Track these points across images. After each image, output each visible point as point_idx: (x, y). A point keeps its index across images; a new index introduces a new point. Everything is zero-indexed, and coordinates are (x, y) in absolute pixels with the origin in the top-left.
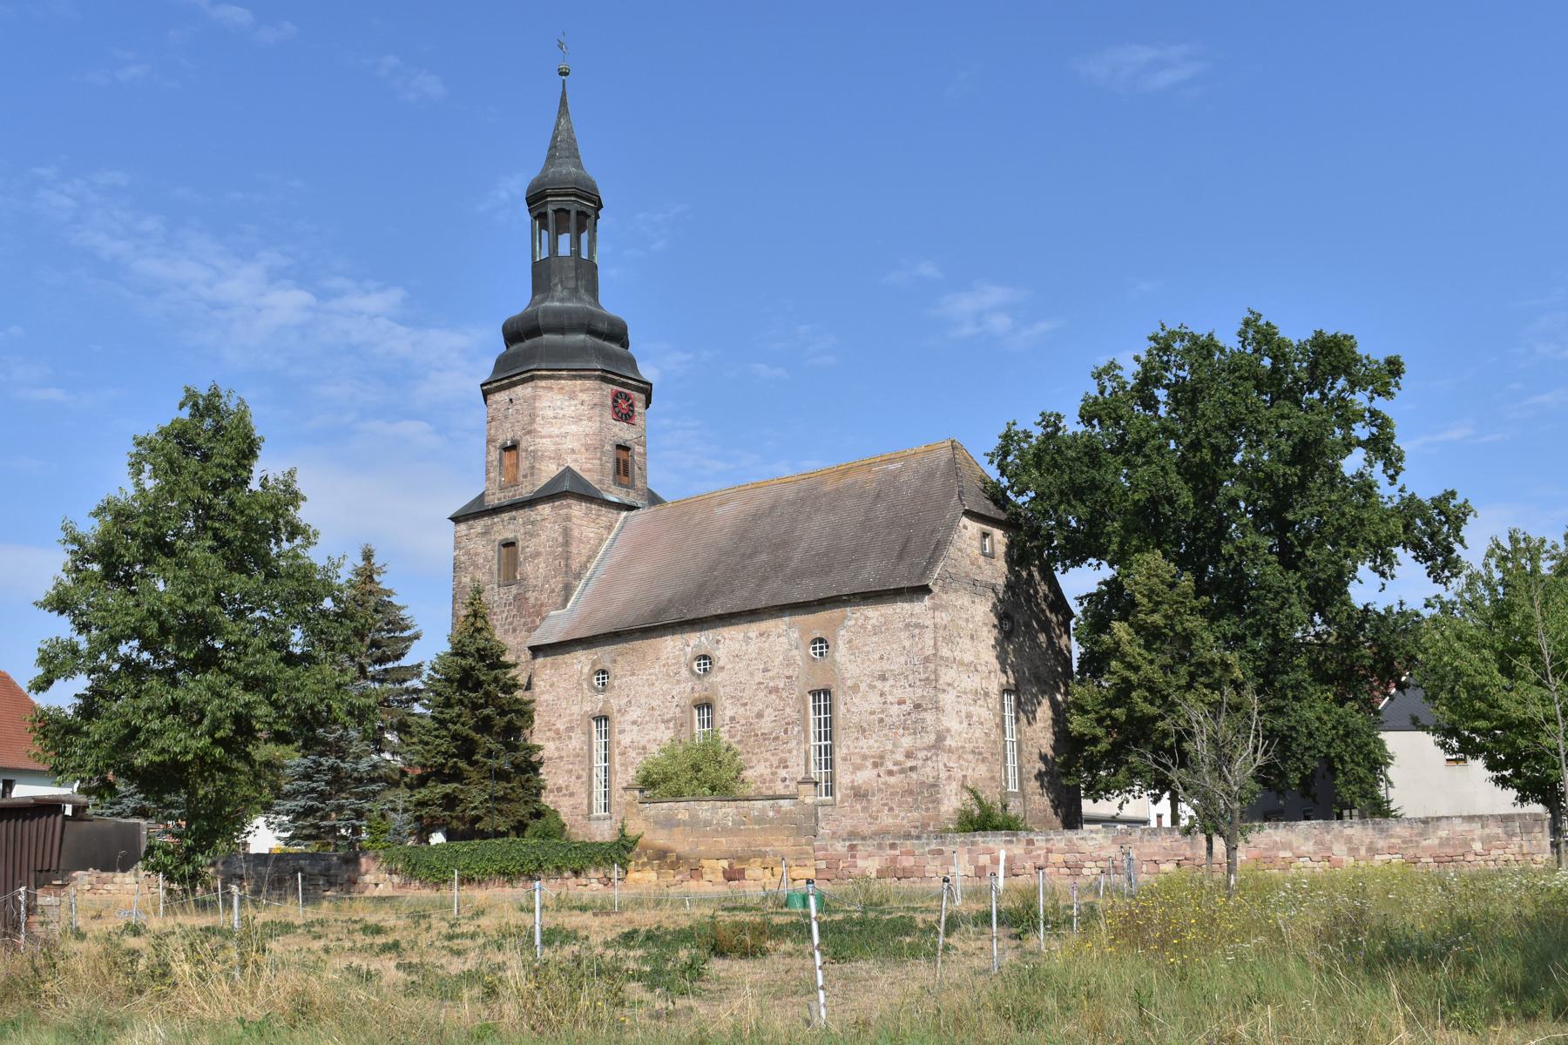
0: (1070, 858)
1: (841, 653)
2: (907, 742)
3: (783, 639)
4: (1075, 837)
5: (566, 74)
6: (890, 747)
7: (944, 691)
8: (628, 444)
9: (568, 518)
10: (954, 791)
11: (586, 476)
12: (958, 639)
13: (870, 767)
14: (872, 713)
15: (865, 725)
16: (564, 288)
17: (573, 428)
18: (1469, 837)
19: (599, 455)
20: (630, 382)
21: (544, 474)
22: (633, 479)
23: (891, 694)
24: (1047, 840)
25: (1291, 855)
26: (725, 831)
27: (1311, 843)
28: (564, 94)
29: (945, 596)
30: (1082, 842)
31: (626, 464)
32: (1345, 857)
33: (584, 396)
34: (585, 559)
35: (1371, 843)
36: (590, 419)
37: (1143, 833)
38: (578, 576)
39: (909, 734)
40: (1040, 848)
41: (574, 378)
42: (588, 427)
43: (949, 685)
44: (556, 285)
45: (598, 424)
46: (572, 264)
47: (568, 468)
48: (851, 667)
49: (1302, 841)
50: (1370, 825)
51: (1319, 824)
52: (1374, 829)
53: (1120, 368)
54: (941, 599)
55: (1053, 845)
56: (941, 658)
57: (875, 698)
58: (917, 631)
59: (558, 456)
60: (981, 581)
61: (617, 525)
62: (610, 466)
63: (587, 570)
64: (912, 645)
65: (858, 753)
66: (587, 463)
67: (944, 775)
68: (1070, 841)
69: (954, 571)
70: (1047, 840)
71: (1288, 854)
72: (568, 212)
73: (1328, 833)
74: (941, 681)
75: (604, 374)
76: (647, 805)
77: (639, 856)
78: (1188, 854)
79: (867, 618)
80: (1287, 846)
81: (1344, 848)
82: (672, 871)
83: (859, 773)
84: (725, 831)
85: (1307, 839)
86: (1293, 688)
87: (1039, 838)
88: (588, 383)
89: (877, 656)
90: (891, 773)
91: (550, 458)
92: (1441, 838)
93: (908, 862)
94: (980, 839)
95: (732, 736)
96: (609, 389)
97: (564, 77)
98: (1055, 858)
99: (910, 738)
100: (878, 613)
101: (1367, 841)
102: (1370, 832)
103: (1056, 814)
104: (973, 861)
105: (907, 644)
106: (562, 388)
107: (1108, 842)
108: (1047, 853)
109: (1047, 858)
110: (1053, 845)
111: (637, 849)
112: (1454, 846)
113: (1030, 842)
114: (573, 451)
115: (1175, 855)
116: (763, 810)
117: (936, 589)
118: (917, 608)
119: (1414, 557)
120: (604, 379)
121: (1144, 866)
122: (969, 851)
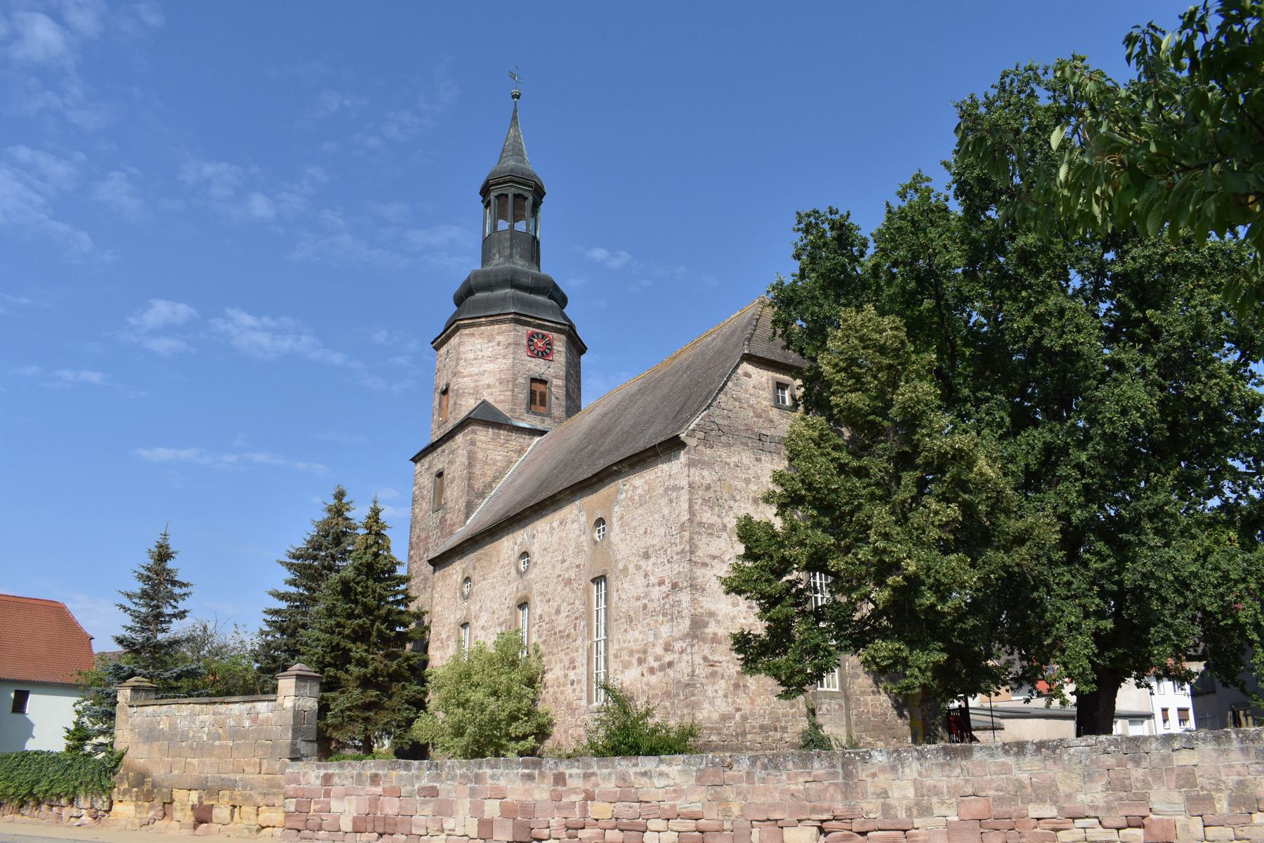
0: (626, 810)
1: (615, 532)
2: (665, 631)
3: (575, 525)
4: (632, 770)
5: (518, 97)
6: (651, 639)
7: (705, 565)
8: (544, 377)
9: (473, 443)
10: (721, 693)
11: (499, 407)
12: (732, 503)
13: (636, 664)
14: (638, 599)
15: (631, 613)
16: (501, 256)
17: (490, 366)
19: (511, 386)
20: (546, 323)
21: (464, 408)
22: (550, 410)
23: (653, 574)
24: (586, 776)
25: (1054, 812)
26: (201, 750)
27: (1099, 786)
28: (515, 111)
29: (708, 451)
30: (644, 780)
31: (543, 396)
32: (1181, 819)
33: (500, 338)
34: (489, 479)
35: (1241, 784)
36: (504, 357)
37: (753, 764)
38: (482, 495)
39: (668, 622)
40: (574, 791)
41: (492, 323)
42: (504, 363)
43: (714, 558)
44: (494, 255)
46: (508, 236)
47: (484, 402)
48: (622, 547)
49: (1077, 782)
50: (1236, 744)
52: (1245, 751)
53: (928, 180)
54: (702, 454)
55: (596, 785)
56: (701, 524)
57: (640, 581)
58: (674, 494)
59: (476, 391)
60: (773, 437)
61: (529, 449)
62: (523, 396)
63: (492, 490)
64: (670, 513)
65: (627, 648)
67: (702, 671)
68: (623, 778)
69: (726, 422)
70: (586, 776)
71: (1049, 811)
72: (506, 196)
73: (1137, 762)
74: (700, 553)
75: (517, 317)
76: (135, 709)
77: (121, 782)
78: (839, 807)
79: (635, 488)
80: (1045, 793)
81: (1178, 797)
82: (147, 804)
83: (627, 672)
84: (201, 750)
85: (1088, 777)
86: (1152, 516)
87: (575, 771)
88: (504, 327)
89: (642, 531)
90: (652, 671)
91: (470, 394)
93: (391, 807)
94: (488, 771)
95: (540, 637)
96: (525, 331)
98: (599, 809)
99: (668, 626)
100: (643, 480)
101: (1232, 780)
102: (1236, 758)
103: (901, 715)
104: (477, 810)
105: (666, 511)
107: (687, 782)
108: (586, 799)
109: (584, 810)
110: (596, 785)
111: (121, 771)
113: (560, 779)
114: (489, 386)
115: (814, 810)
116: (239, 719)
117: (692, 442)
118: (674, 467)
120: (517, 322)
121: (755, 831)
122: (473, 793)
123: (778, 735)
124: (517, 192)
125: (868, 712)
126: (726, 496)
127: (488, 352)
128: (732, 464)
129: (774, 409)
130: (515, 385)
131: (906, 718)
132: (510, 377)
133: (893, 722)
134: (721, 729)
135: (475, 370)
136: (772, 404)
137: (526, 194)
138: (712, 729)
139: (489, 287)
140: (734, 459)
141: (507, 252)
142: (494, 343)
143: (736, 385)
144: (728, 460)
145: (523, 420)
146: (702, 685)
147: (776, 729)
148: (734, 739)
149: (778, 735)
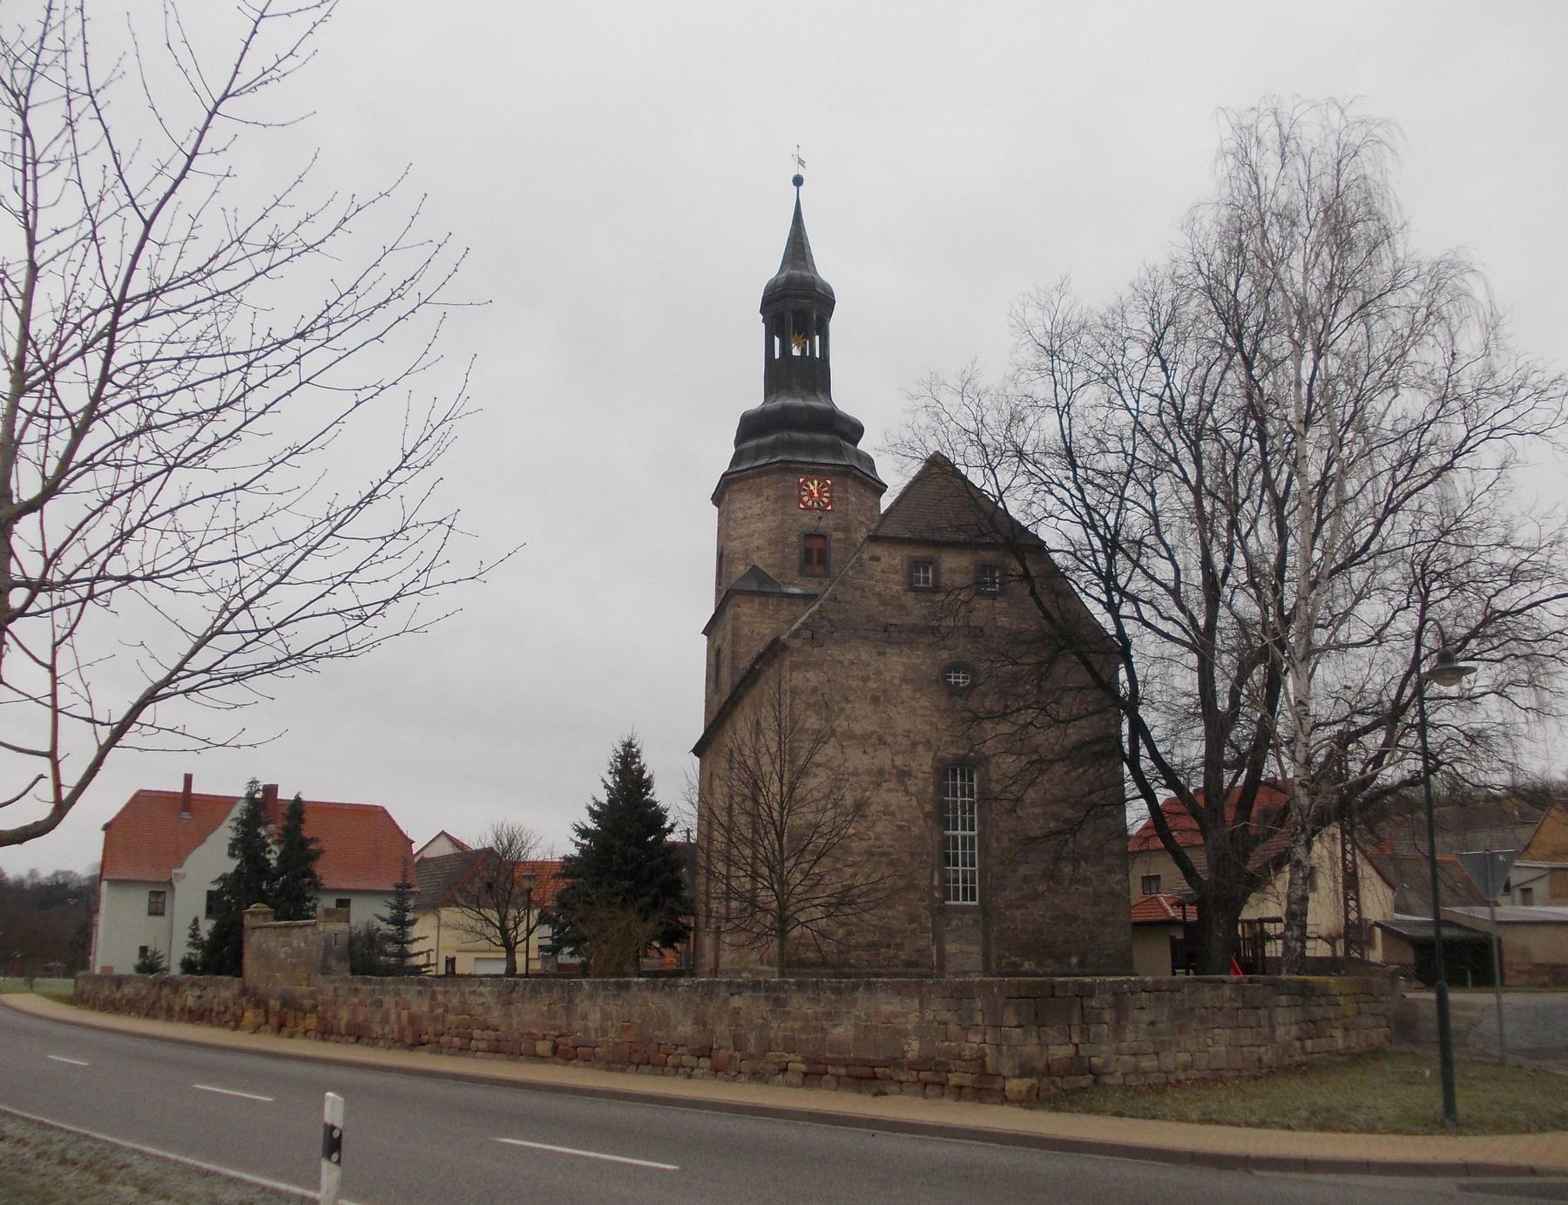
8: (821, 531)
29: (816, 651)
33: (769, 492)
62: (795, 557)
123: (892, 952)
125: (1016, 928)
126: (836, 698)
127: (756, 510)
129: (909, 594)
135: (743, 531)
136: (906, 587)
140: (850, 656)
142: (762, 498)
144: (841, 658)
147: (888, 946)
148: (835, 957)
149: (892, 952)
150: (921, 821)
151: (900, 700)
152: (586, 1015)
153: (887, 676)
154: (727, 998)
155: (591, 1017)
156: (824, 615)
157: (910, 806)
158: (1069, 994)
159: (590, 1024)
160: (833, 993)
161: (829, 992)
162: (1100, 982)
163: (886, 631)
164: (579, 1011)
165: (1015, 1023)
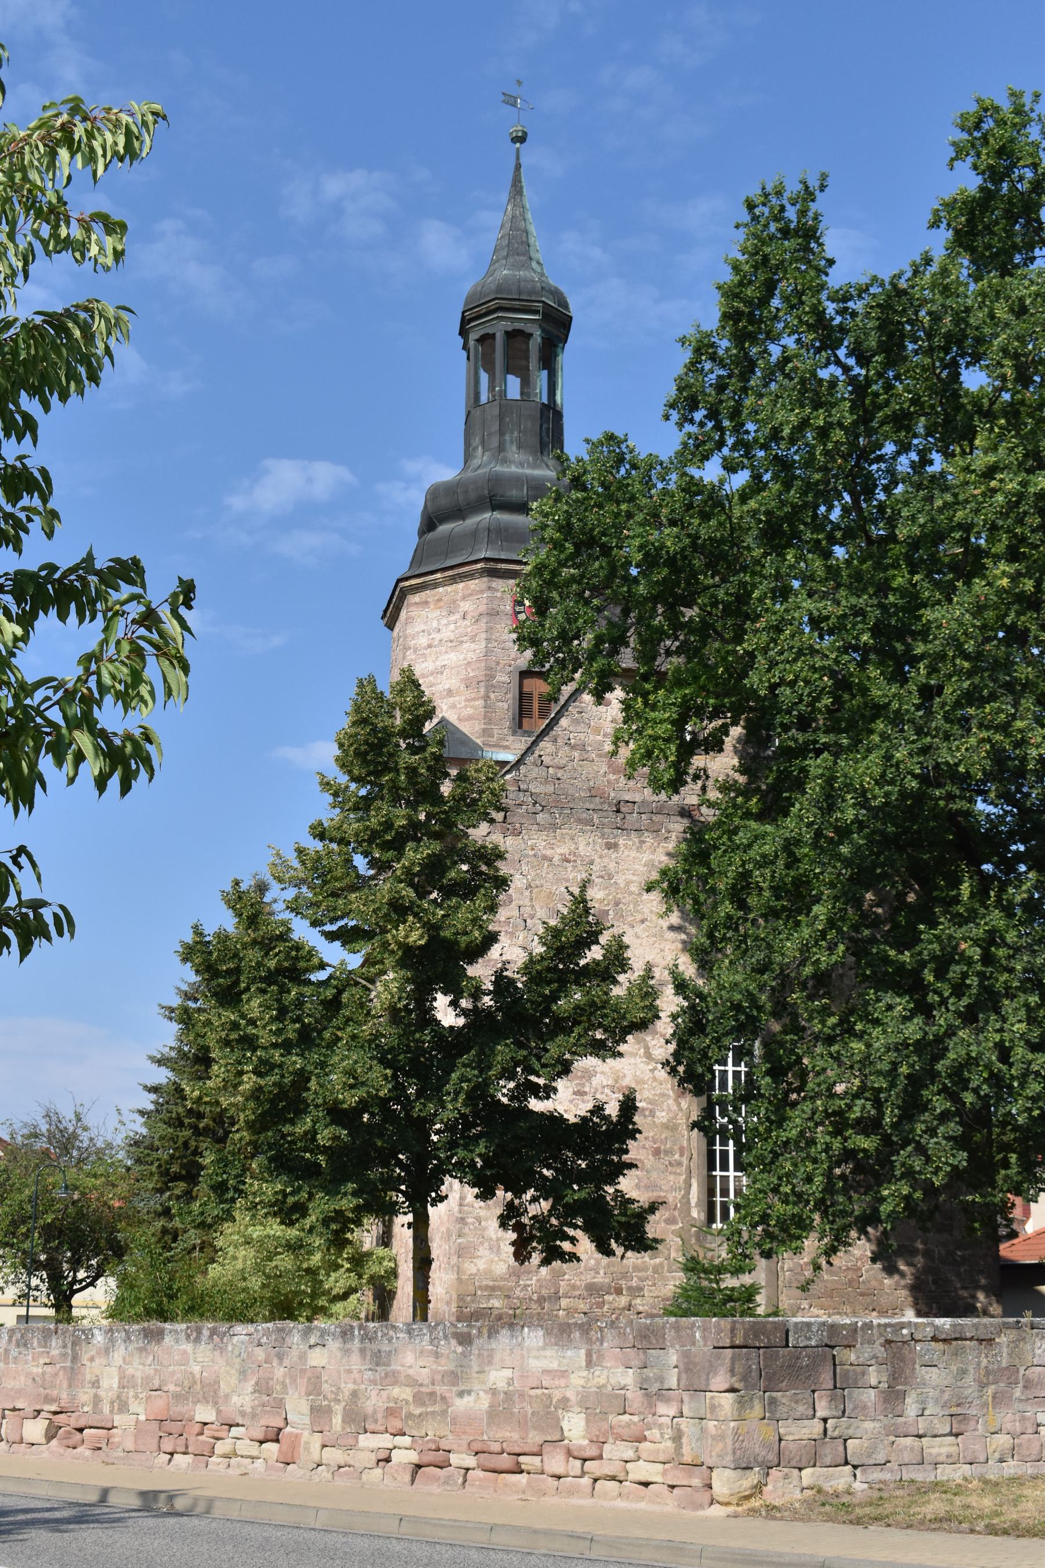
11: (466, 728)
17: (452, 658)
18: (557, 1395)
19: (482, 690)
28: (518, 167)
33: (465, 606)
36: (473, 639)
41: (454, 580)
42: (472, 651)
45: (484, 644)
51: (267, 1333)
62: (506, 705)
66: (466, 707)
69: (550, 789)
71: (205, 1413)
72: (493, 336)
88: (473, 584)
92: (494, 1392)
97: (518, 145)
106: (439, 600)
112: (522, 1424)
114: (450, 693)
119: (90, 558)
120: (493, 573)
123: (623, 1301)
124: (510, 326)
128: (556, 859)
130: (490, 687)
131: (903, 1275)
132: (481, 674)
133: (874, 1283)
134: (510, 1289)
137: (529, 328)
138: (493, 1289)
139: (458, 513)
140: (563, 849)
141: (495, 442)
142: (457, 616)
143: (576, 722)
144: (549, 853)
145: (506, 747)
146: (479, 1220)
147: (619, 1291)
149: (623, 1301)
150: (671, 1102)
151: (639, 917)
152: (98, 1381)
153: (621, 880)
154: (305, 1353)
155: (104, 1383)
156: (523, 786)
157: (655, 1079)
158: (813, 1343)
159: (102, 1393)
160: (460, 1343)
161: (453, 1342)
162: (865, 1324)
163: (618, 811)
164: (88, 1377)
165: (726, 1386)
